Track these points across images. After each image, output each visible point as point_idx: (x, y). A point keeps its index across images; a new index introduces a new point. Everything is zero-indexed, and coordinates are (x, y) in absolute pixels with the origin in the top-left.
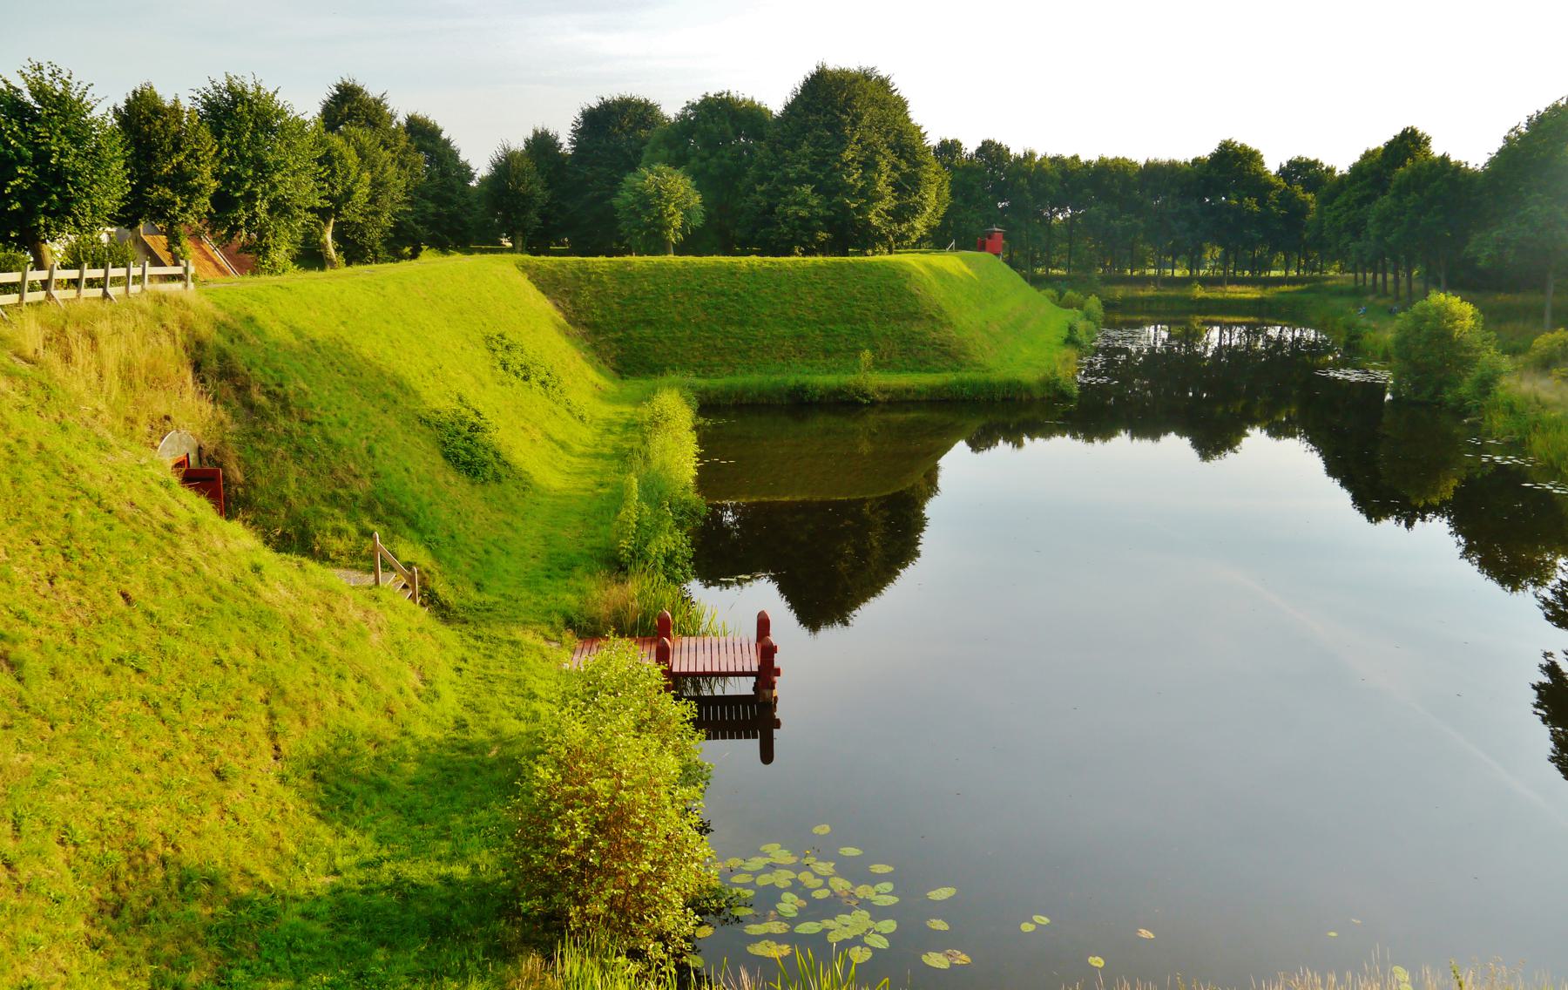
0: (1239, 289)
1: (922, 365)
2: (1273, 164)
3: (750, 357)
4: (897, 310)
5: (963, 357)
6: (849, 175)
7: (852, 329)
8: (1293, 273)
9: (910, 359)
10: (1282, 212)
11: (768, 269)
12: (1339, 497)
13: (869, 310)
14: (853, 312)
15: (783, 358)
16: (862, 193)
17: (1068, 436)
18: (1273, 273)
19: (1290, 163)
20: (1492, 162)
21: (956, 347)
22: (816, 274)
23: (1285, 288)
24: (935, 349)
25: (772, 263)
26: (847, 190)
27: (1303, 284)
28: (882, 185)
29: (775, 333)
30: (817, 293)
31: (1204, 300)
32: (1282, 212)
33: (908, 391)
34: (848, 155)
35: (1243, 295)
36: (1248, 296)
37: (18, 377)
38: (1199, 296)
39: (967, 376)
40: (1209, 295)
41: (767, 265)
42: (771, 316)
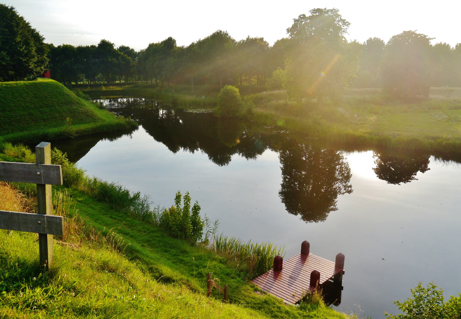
0: (114, 87)
1: (81, 121)
2: (116, 47)
3: (13, 125)
4: (64, 101)
5: (94, 116)
6: (21, 48)
7: (50, 110)
8: (122, 82)
9: (76, 119)
10: (124, 63)
11: (5, 87)
12: (162, 147)
13: (53, 101)
14: (48, 103)
15: (27, 124)
16: (26, 55)
17: (368, 151)
18: (117, 82)
19: (120, 47)
20: (59, 47)
21: (90, 113)
22: (27, 88)
23: (127, 86)
24: (83, 114)
25: (6, 84)
26: (20, 54)
27: (132, 85)
28: (33, 52)
29: (20, 114)
30: (31, 96)
31: (106, 91)
32: (124, 63)
33: (85, 131)
34: (18, 39)
35: (115, 89)
36: (118, 89)
37: (214, 251)
38: (104, 90)
39: (99, 124)
40: (107, 90)
41: (4, 85)
42: (15, 107)
